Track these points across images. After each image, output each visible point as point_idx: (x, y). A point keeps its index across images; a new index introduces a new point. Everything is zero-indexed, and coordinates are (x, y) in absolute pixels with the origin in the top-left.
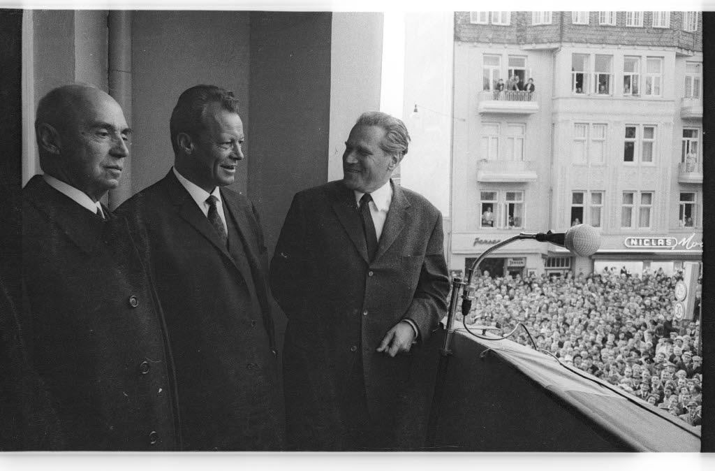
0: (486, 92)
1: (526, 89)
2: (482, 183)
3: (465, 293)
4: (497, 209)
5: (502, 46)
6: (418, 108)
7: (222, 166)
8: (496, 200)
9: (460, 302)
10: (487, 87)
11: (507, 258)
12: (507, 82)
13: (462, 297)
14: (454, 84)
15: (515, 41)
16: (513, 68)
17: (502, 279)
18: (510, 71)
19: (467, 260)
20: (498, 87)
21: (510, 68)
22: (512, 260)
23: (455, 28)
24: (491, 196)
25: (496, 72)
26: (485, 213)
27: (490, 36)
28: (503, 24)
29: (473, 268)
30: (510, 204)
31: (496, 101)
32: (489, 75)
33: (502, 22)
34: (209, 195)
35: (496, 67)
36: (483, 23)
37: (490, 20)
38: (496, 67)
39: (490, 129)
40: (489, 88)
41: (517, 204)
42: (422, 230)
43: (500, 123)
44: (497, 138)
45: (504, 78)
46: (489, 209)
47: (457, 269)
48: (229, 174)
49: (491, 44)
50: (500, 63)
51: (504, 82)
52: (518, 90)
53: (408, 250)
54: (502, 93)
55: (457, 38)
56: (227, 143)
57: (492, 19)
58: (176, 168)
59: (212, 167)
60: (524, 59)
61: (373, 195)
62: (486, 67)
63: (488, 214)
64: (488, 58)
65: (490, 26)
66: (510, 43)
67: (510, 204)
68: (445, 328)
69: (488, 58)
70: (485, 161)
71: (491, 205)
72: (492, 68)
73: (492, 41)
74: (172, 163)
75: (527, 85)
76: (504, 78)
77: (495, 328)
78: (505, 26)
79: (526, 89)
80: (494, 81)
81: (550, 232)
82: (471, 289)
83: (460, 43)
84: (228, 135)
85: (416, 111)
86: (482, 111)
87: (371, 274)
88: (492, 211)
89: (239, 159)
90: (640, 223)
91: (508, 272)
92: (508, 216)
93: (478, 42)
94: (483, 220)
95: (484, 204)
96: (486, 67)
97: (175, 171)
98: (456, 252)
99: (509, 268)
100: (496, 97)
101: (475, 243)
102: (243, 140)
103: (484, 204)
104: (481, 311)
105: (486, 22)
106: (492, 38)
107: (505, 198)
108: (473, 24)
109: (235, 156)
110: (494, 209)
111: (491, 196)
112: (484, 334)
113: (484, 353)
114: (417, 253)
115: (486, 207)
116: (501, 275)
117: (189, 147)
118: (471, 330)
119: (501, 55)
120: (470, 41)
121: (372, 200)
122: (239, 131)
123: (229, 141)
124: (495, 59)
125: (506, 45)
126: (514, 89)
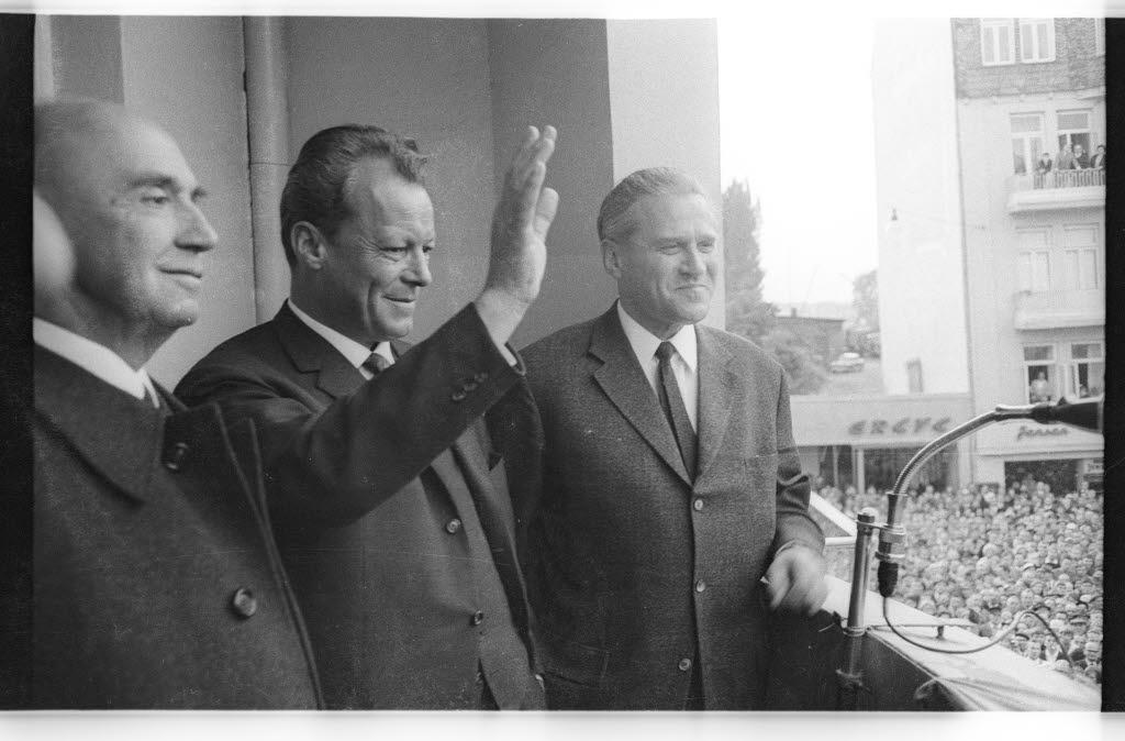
0: (1019, 178)
1: (1093, 165)
2: (1025, 332)
3: (885, 547)
4: (1055, 377)
5: (1043, 97)
6: (898, 214)
7: (387, 297)
8: (1052, 358)
9: (875, 563)
10: (1020, 168)
11: (1081, 460)
12: (1059, 157)
13: (877, 556)
14: (961, 170)
15: (1068, 87)
16: (1068, 132)
17: (1075, 495)
18: (1062, 139)
19: (1007, 465)
20: (1046, 166)
21: (1063, 132)
22: (1092, 463)
23: (956, 77)
24: (1043, 352)
25: (1035, 144)
26: (1035, 382)
27: (1021, 83)
28: (1042, 61)
29: (897, 491)
30: (1080, 365)
31: (1038, 191)
32: (1022, 150)
33: (1041, 56)
34: (370, 353)
35: (1034, 134)
36: (1005, 63)
37: (1018, 55)
38: (1034, 134)
39: (1034, 240)
40: (1024, 171)
41: (1093, 364)
42: (762, 403)
43: (1050, 226)
44: (1047, 253)
45: (1052, 150)
46: (1042, 375)
47: (993, 480)
48: (400, 314)
49: (1023, 96)
50: (1042, 127)
51: (1053, 157)
52: (1079, 168)
53: (749, 449)
54: (1050, 176)
55: (961, 93)
56: (401, 249)
57: (1022, 55)
58: (294, 302)
59: (364, 299)
60: (1086, 115)
61: (675, 341)
62: (1019, 135)
63: (1040, 384)
64: (1019, 121)
65: (1019, 66)
66: (1059, 89)
67: (1080, 365)
68: (844, 624)
69: (1019, 121)
70: (1029, 293)
71: (1043, 369)
72: (1027, 136)
73: (1025, 91)
74: (287, 294)
75: (1095, 157)
76: (1052, 150)
77: (968, 623)
78: (1047, 63)
79: (1093, 165)
80: (1034, 160)
81: (1062, 401)
82: (898, 538)
83: (966, 100)
84: (400, 230)
85: (895, 218)
86: (1017, 209)
87: (699, 504)
88: (1046, 378)
89: (420, 284)
90: (1062, 111)
91: (1085, 484)
92: (1078, 385)
93: (999, 95)
94: (1031, 395)
95: (1031, 368)
96: (1019, 135)
97: (293, 307)
98: (988, 453)
99: (1086, 477)
100: (1039, 184)
101: (1020, 435)
102: (432, 244)
103: (1031, 368)
104: (1036, 555)
105: (1012, 61)
106: (1025, 87)
107: (1070, 353)
108: (986, 68)
109: (412, 277)
110: (1050, 374)
111: (1043, 352)
112: (940, 636)
113: (926, 689)
114: (764, 450)
115: (1034, 373)
116: (1072, 487)
117: (317, 255)
118: (897, 629)
119: (1043, 112)
120: (985, 95)
121: (675, 351)
122: (424, 223)
123: (402, 245)
124: (1032, 121)
125: (1051, 95)
126: (1073, 167)
